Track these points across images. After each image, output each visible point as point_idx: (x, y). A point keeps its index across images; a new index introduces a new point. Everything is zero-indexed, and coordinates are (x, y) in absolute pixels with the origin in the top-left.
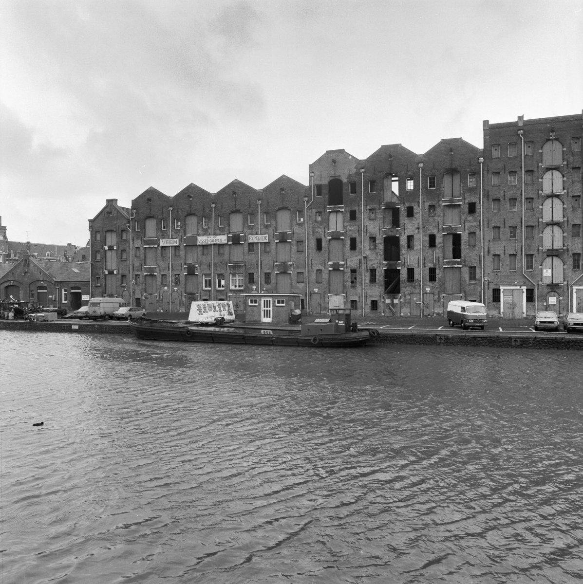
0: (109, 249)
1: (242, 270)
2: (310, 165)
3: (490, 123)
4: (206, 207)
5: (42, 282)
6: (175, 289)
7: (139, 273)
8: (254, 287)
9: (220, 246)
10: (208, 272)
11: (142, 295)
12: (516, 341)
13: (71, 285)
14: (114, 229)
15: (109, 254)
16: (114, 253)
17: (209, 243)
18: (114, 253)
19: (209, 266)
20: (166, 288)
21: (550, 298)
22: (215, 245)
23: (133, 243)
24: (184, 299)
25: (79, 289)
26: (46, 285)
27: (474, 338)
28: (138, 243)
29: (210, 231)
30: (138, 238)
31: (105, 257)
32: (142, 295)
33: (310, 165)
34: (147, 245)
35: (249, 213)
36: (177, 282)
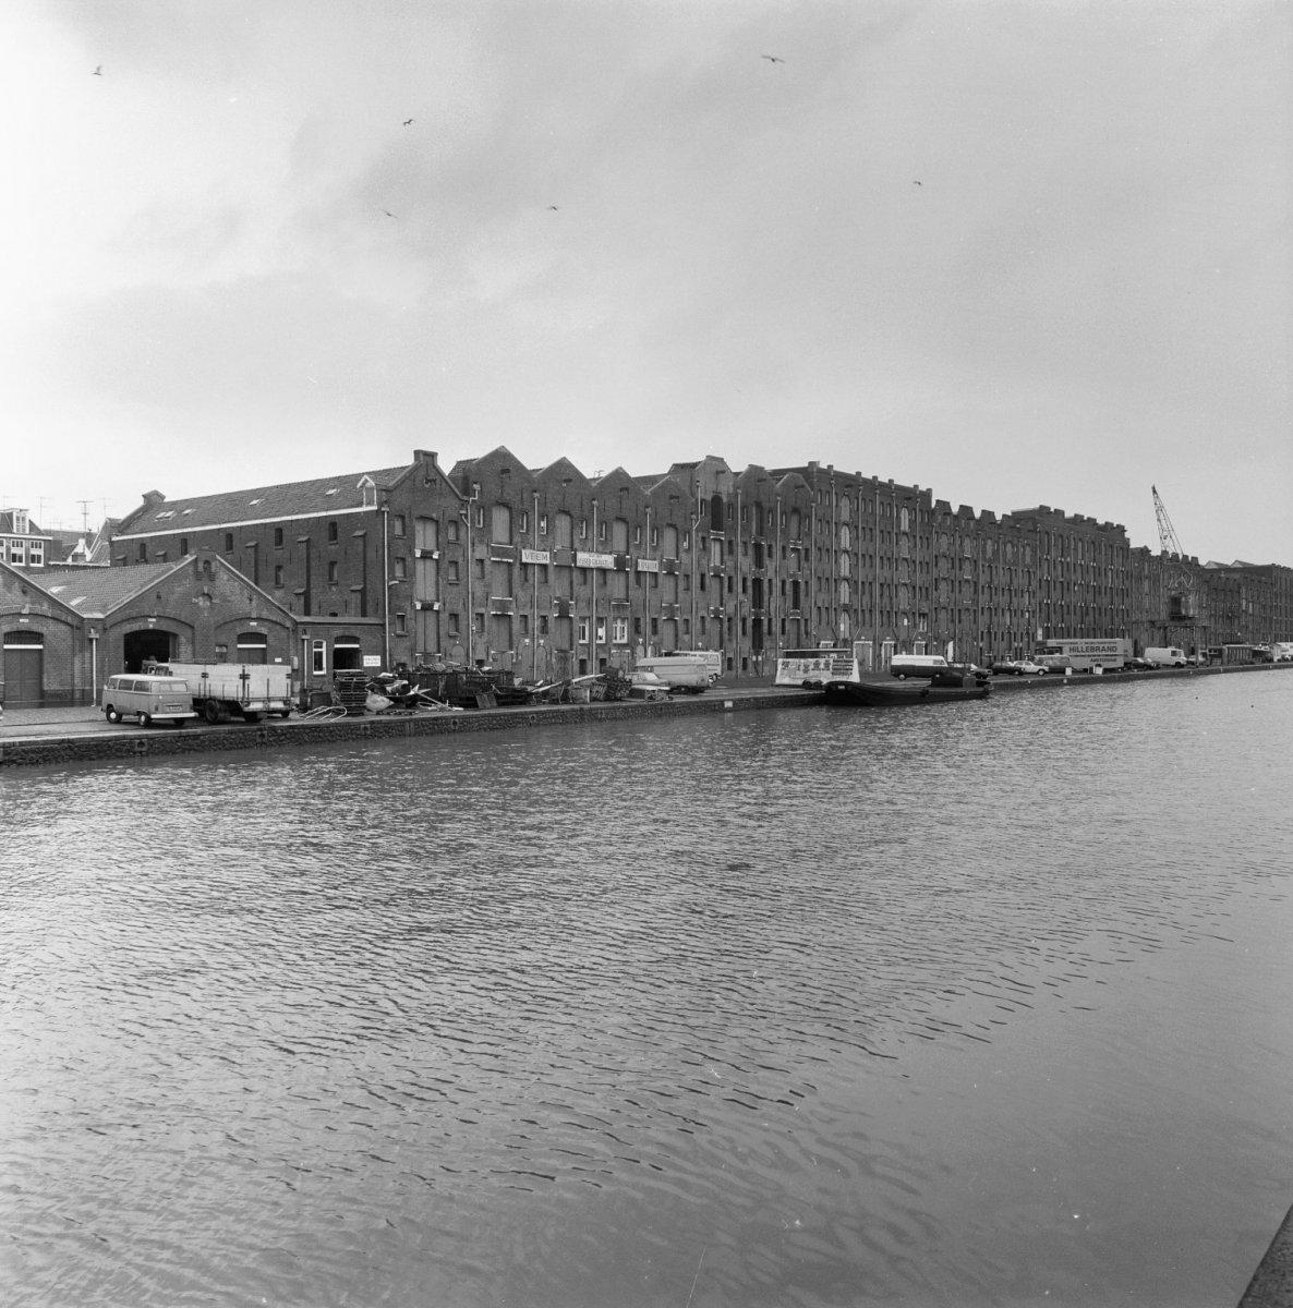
0: (422, 557)
1: (628, 613)
2: (1121, 529)
3: (835, 469)
4: (584, 503)
5: (254, 624)
6: (542, 641)
7: (482, 610)
8: (641, 640)
9: (603, 571)
10: (587, 614)
11: (488, 654)
12: (141, 744)
13: (338, 632)
14: (434, 515)
15: (420, 566)
16: (430, 566)
17: (592, 565)
18: (430, 566)
19: (589, 602)
20: (527, 641)
21: (365, 657)
22: (599, 569)
23: (473, 551)
24: (554, 660)
25: (355, 640)
26: (264, 631)
27: (1020, 683)
28: (481, 552)
29: (589, 544)
30: (481, 542)
31: (409, 575)
32: (488, 654)
33: (1121, 529)
34: (498, 556)
35: (579, 519)
36: (544, 630)
